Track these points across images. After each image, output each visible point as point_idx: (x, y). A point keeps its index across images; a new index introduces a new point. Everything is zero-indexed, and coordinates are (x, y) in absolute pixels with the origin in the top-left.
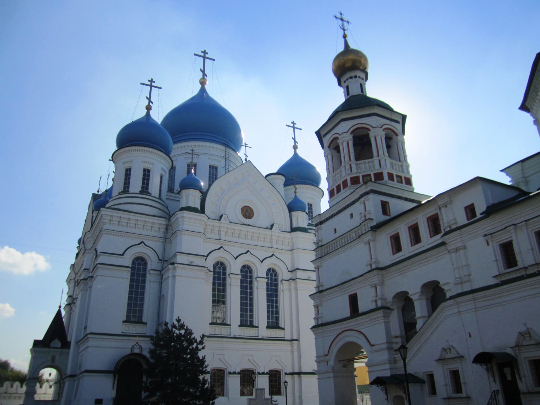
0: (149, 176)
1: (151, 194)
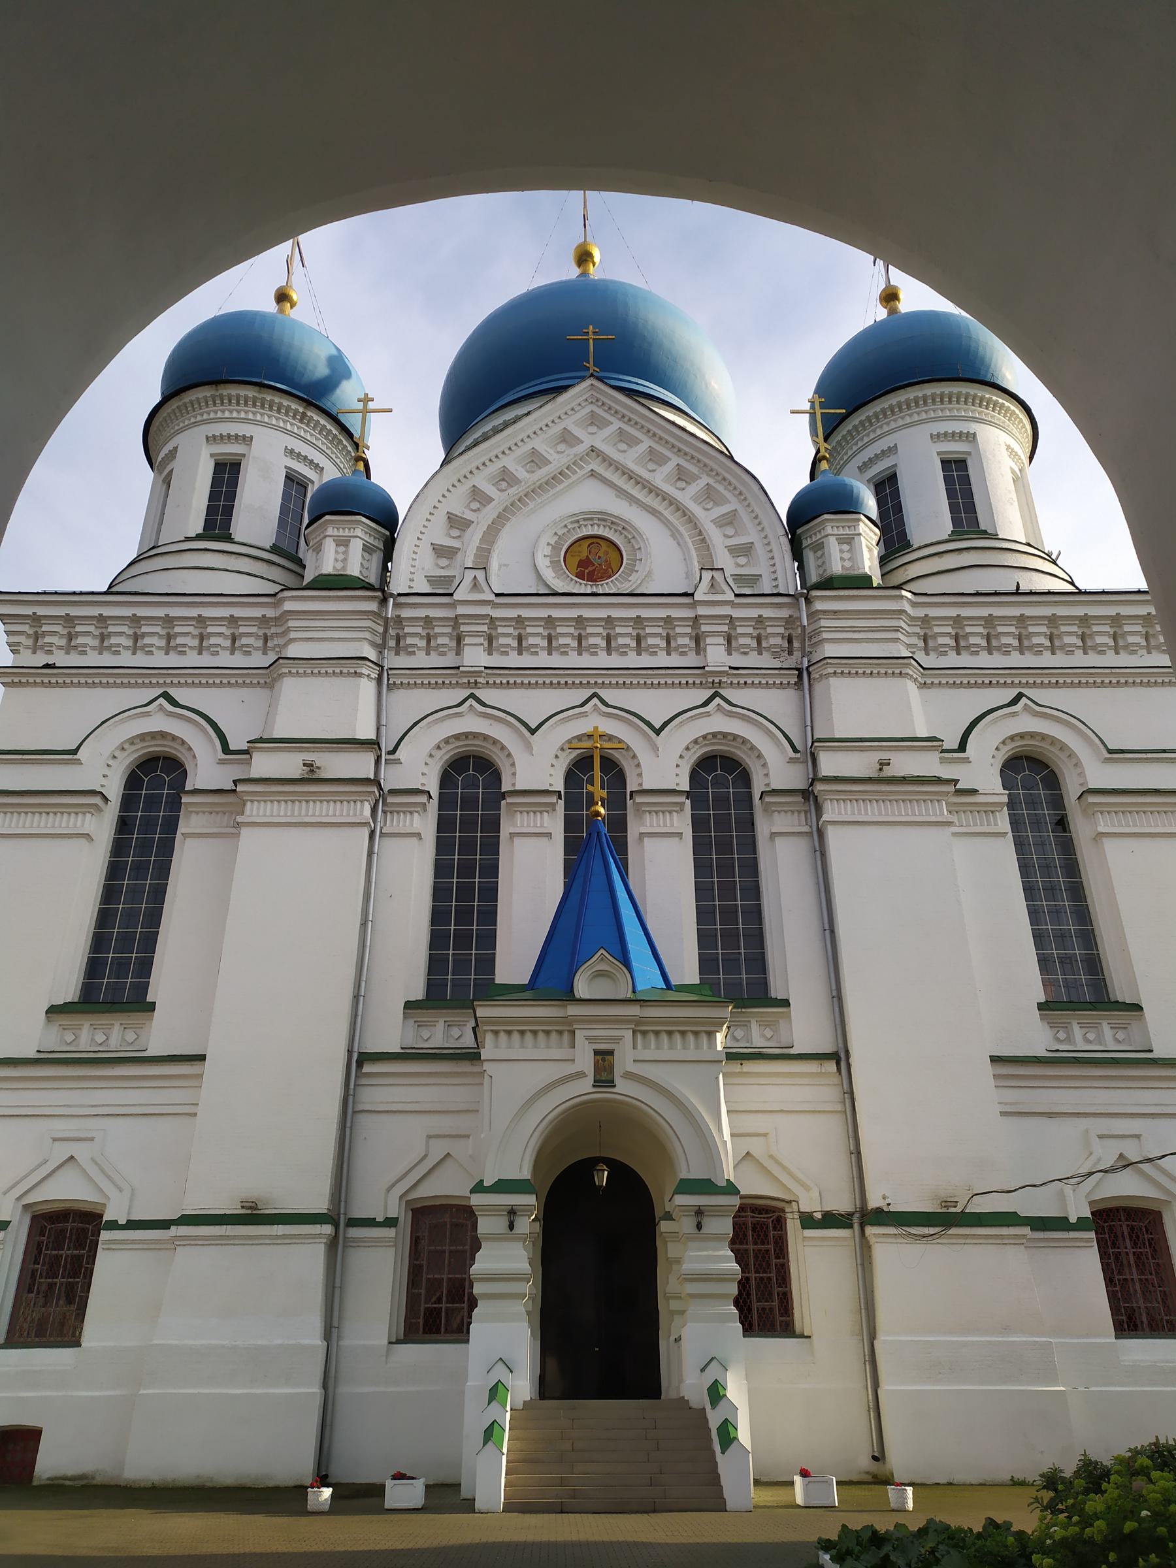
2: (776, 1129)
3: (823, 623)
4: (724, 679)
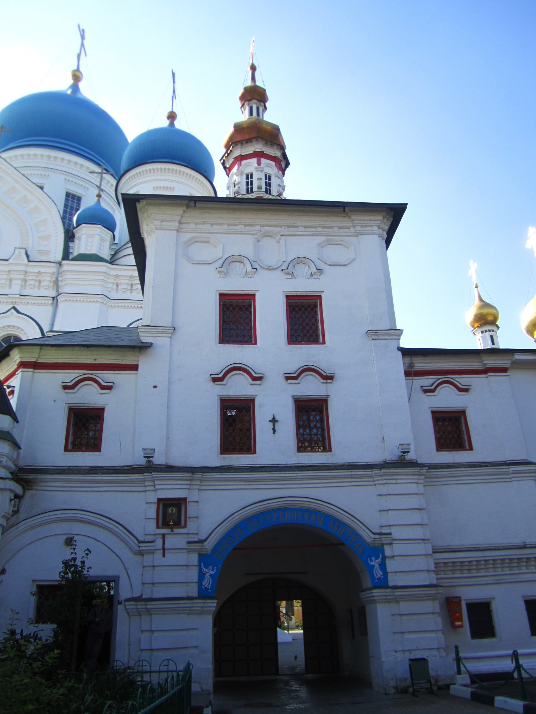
2: (380, 511)
3: (67, 276)
4: (17, 301)
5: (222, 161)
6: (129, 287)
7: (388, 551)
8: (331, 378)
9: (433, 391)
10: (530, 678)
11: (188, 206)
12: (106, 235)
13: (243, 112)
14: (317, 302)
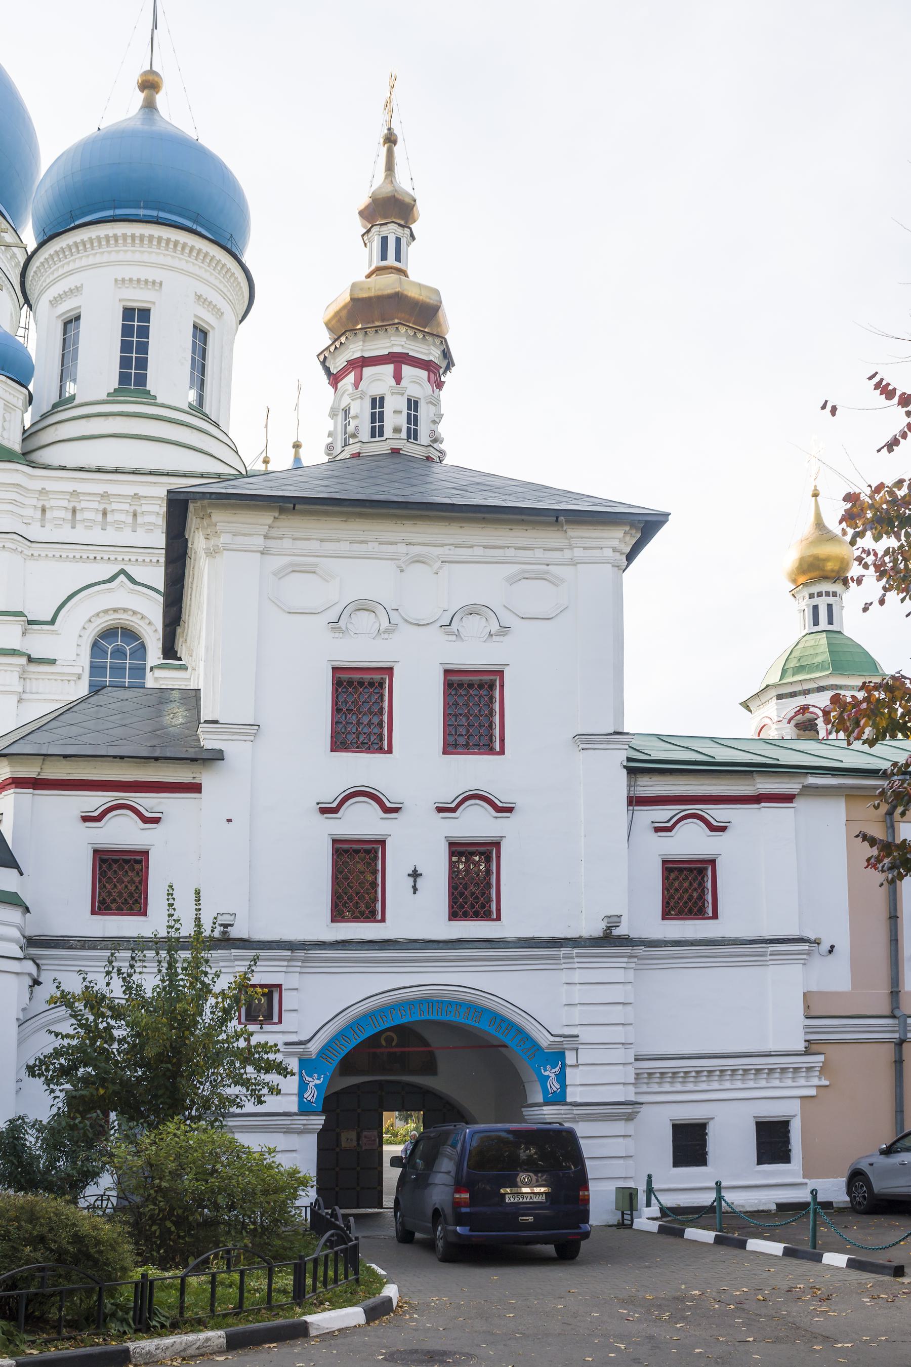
0: (144, 332)
1: (155, 397)
5: (322, 358)
6: (69, 516)
7: (570, 1058)
8: (510, 810)
9: (669, 829)
10: (731, 1213)
11: (282, 510)
12: (14, 396)
13: (365, 244)
14: (496, 680)
